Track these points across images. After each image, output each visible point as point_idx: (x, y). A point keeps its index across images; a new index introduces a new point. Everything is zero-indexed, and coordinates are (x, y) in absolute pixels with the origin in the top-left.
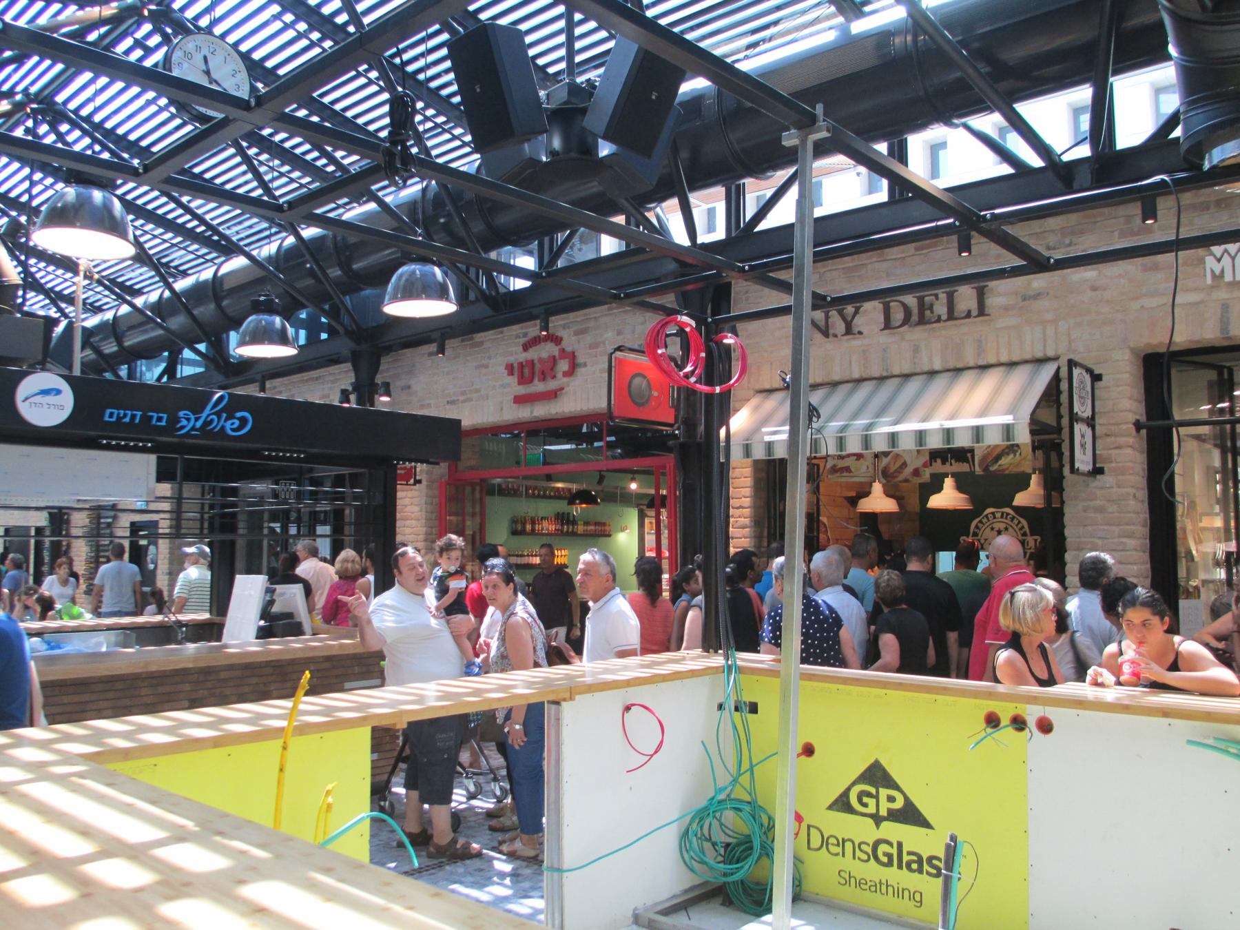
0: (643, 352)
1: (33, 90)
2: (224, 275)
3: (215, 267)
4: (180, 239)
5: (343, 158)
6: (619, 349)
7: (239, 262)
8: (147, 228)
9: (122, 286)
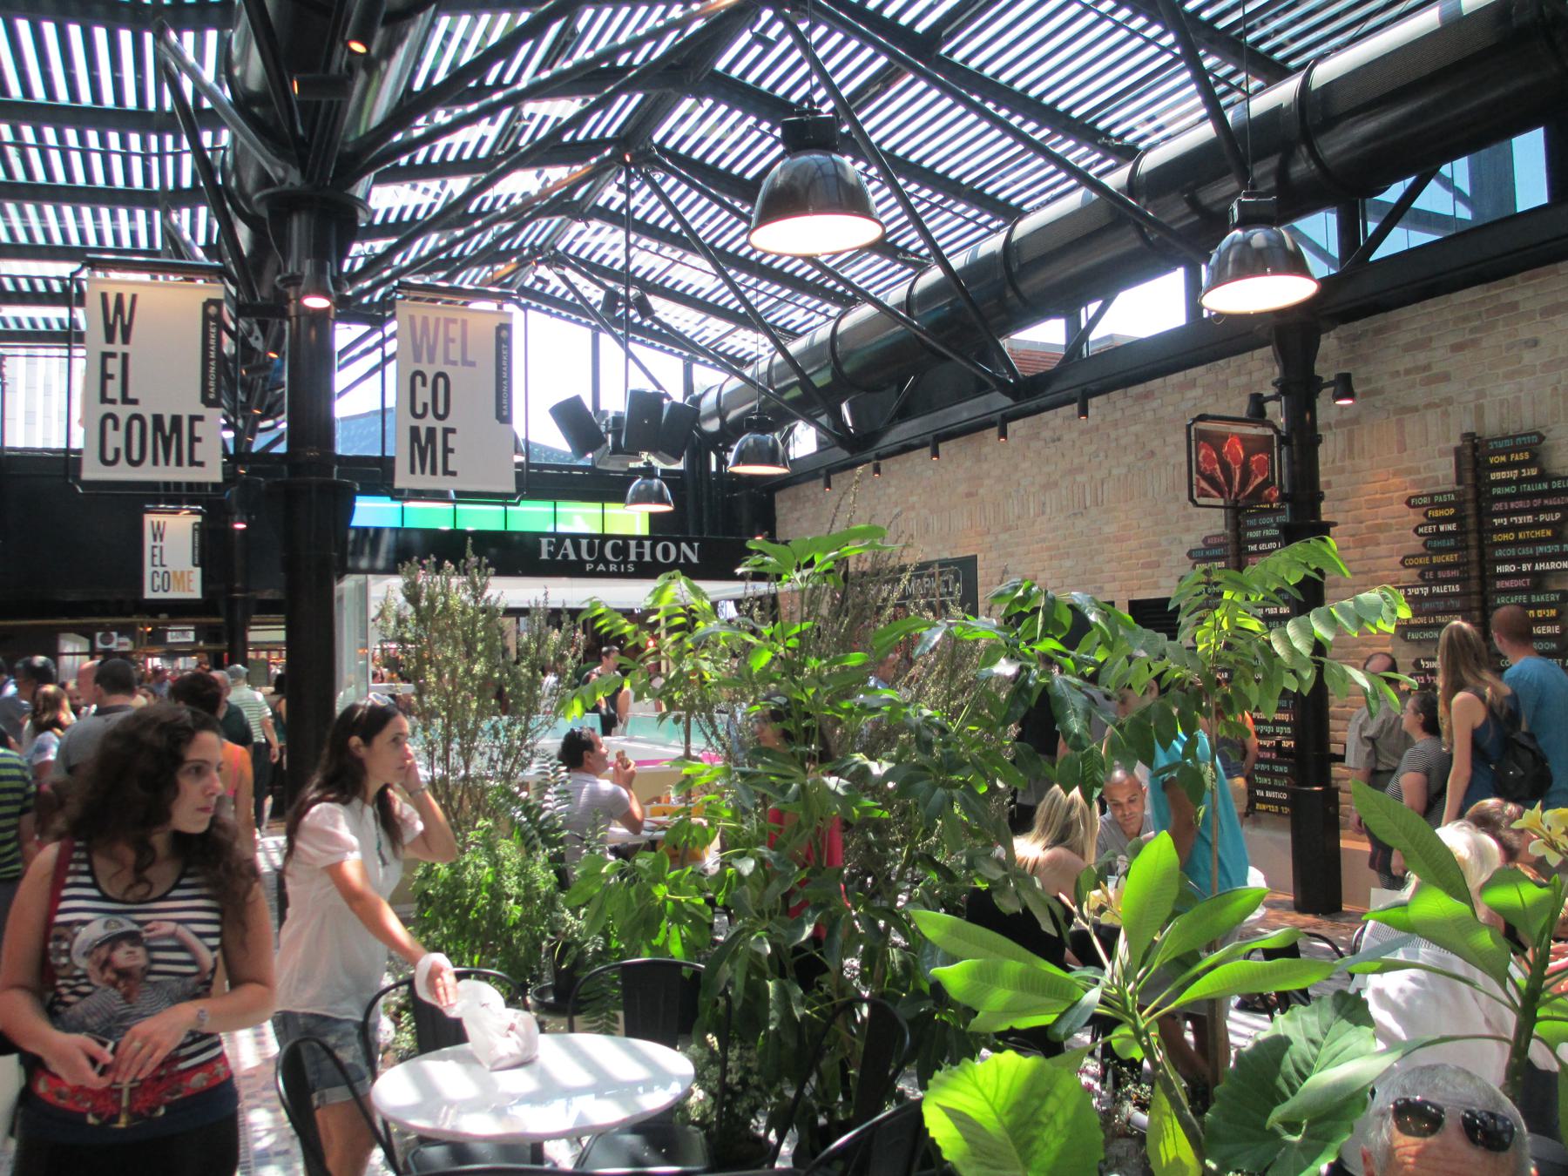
0: (510, 612)
1: (538, 243)
2: (1021, 239)
3: (832, 323)
4: (787, 291)
5: (1034, 132)
6: (1195, 420)
7: (865, 311)
8: (760, 287)
9: (732, 358)
